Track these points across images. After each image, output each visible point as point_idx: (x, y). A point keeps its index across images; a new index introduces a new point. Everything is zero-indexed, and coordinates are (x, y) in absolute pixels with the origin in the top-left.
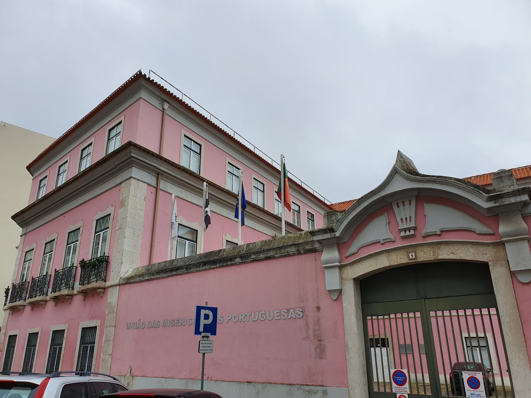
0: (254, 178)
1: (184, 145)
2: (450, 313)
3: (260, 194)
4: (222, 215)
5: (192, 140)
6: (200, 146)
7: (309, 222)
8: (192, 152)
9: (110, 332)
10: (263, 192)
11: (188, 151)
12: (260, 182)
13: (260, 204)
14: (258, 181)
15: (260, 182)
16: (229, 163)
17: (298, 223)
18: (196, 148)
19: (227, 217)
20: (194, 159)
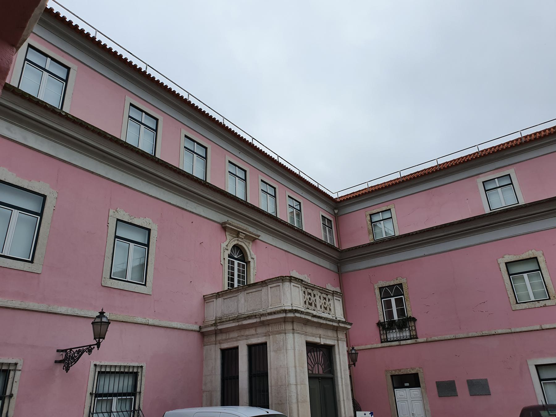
0: (289, 196)
1: (229, 172)
2: (293, 327)
3: (270, 200)
4: (108, 179)
5: (194, 141)
6: (206, 148)
7: (325, 229)
8: (195, 155)
9: (272, 343)
10: (275, 197)
11: (233, 177)
12: (270, 185)
13: (271, 211)
14: (267, 184)
15: (270, 185)
16: (229, 162)
17: (298, 222)
18: (241, 174)
19: (121, 184)
20: (240, 185)
